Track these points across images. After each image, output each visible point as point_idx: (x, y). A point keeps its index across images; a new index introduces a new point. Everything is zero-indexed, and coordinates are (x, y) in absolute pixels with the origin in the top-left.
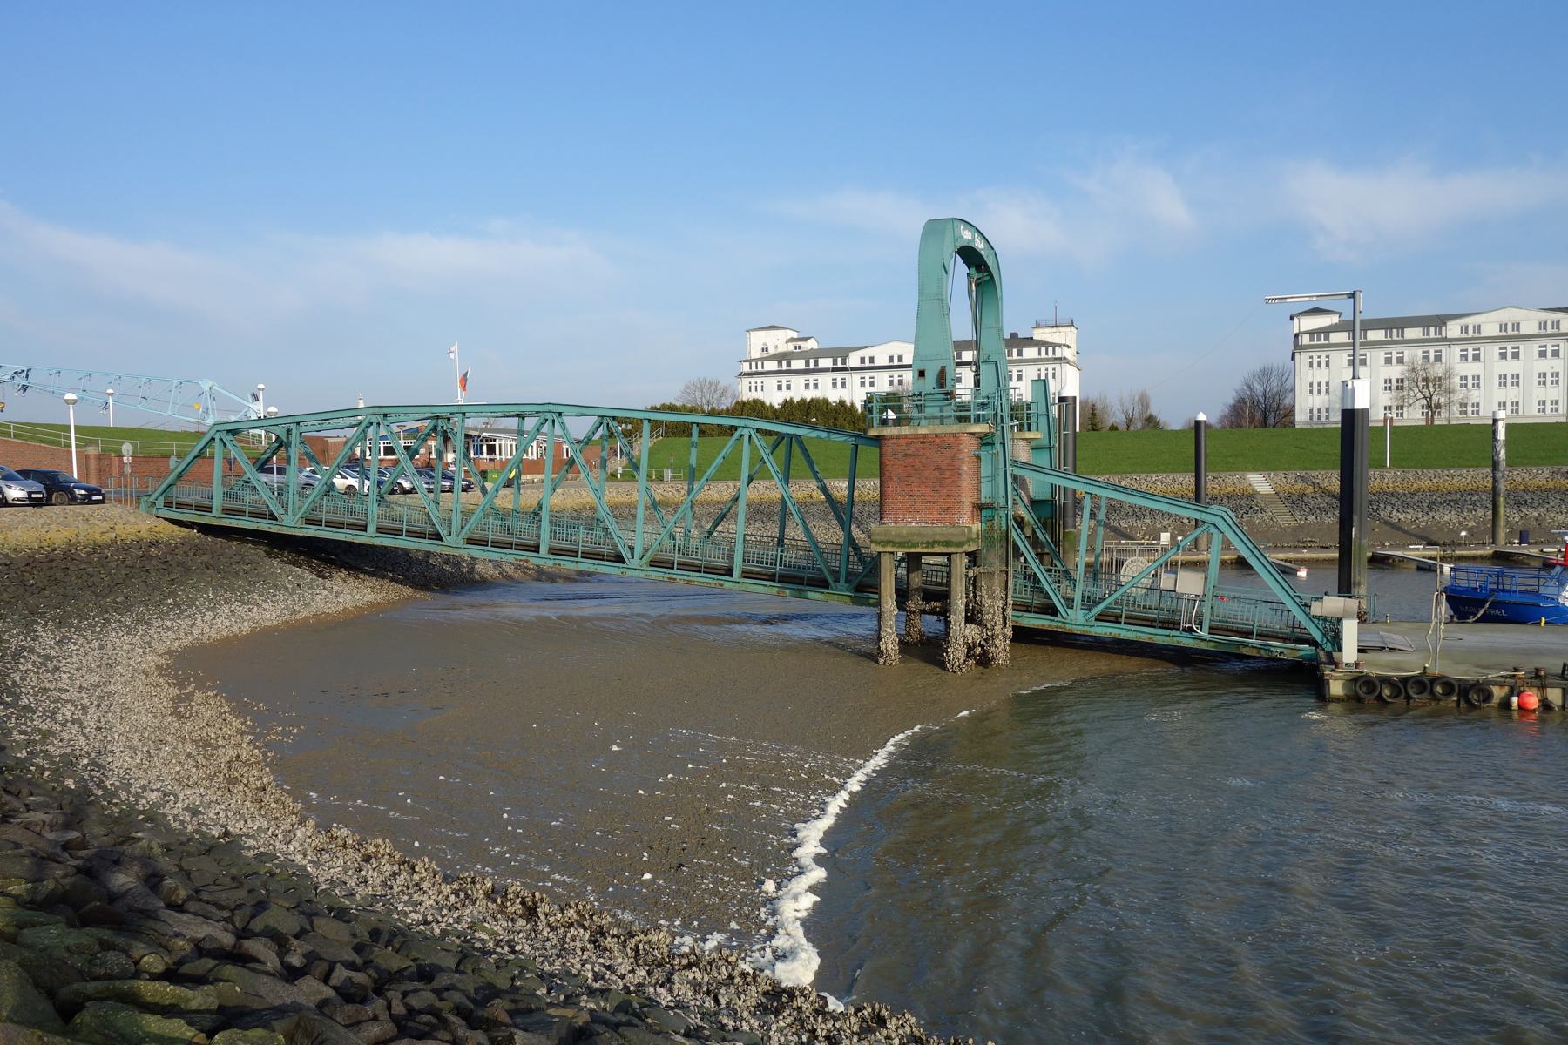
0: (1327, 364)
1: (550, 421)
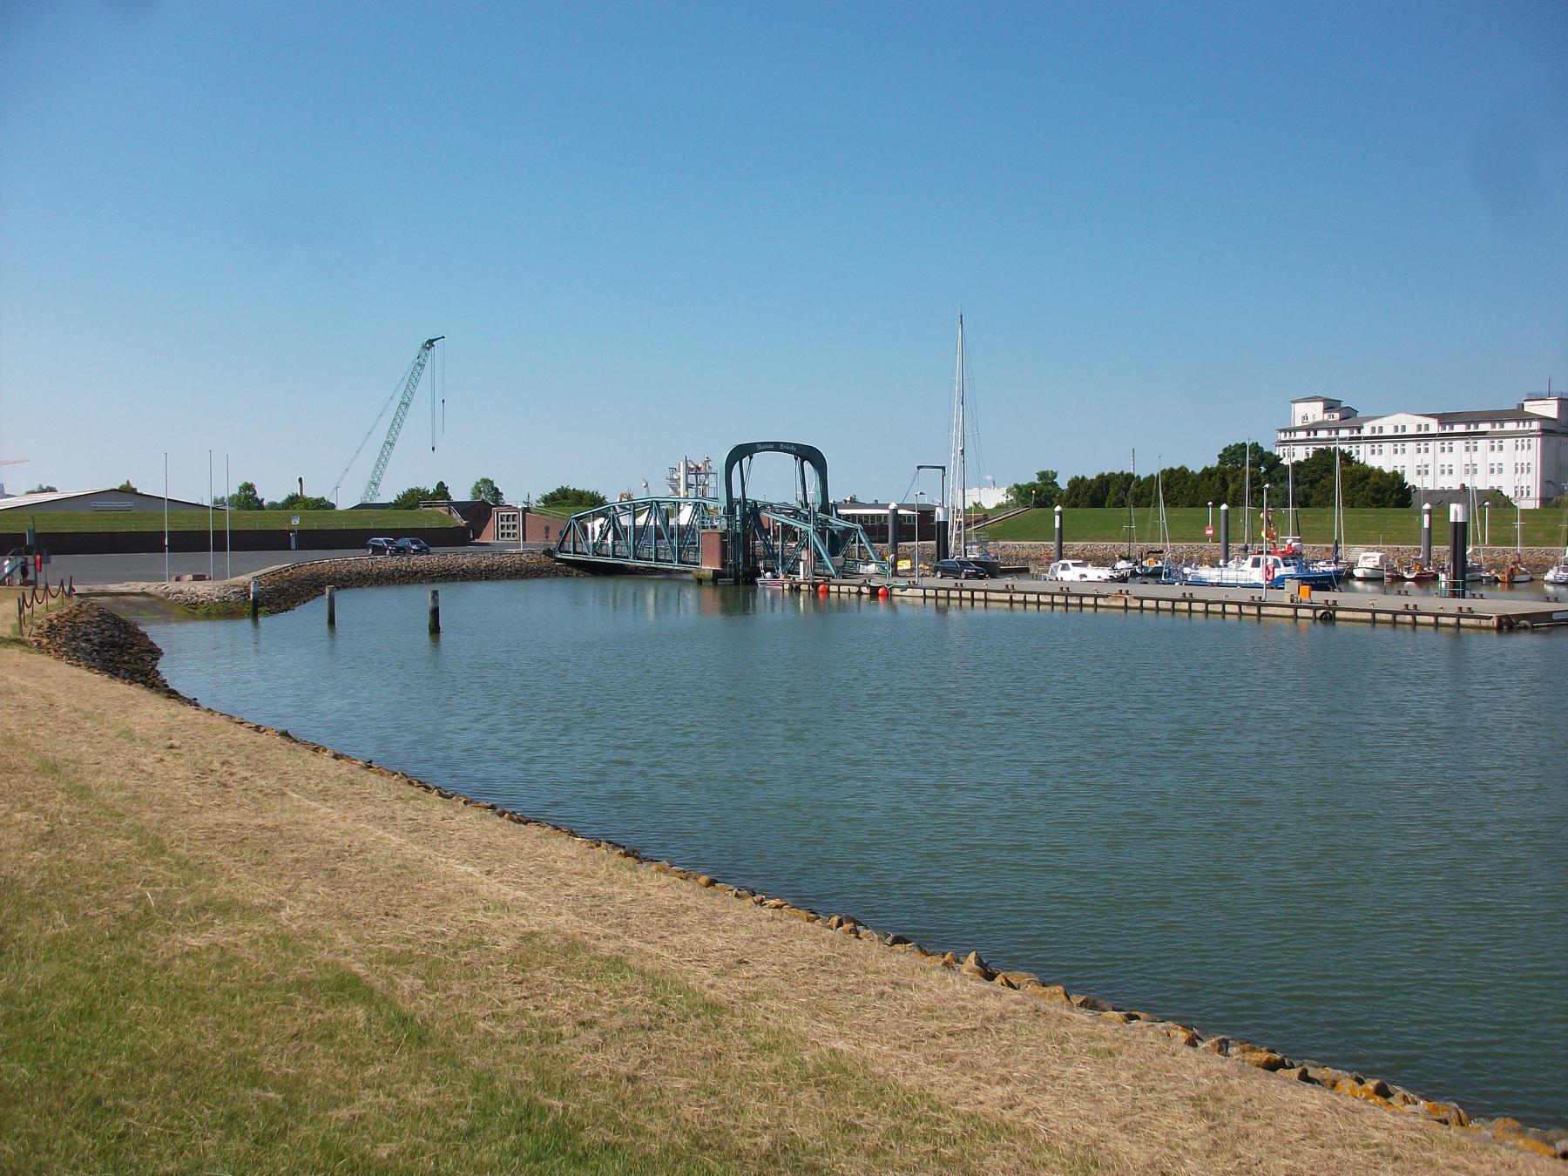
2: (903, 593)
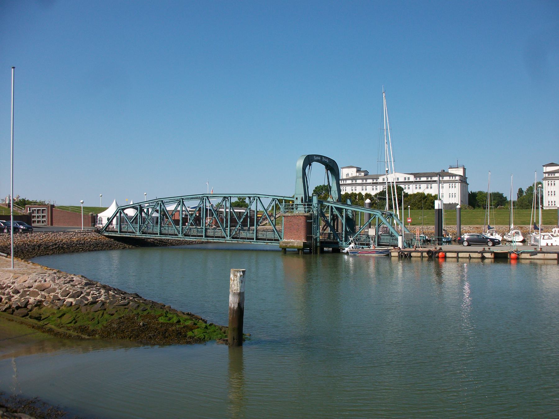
1: (256, 200)
2: (532, 257)
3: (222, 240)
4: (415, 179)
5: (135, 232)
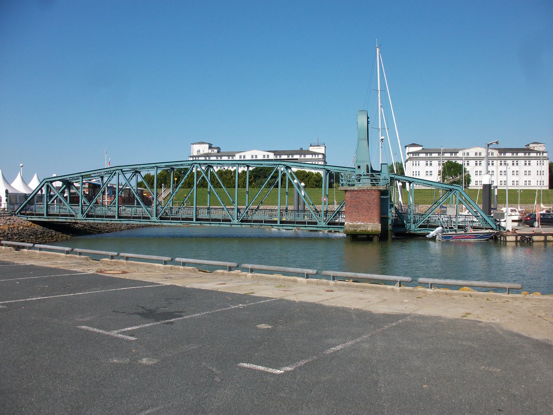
0: (419, 165)
1: (117, 174)
3: (144, 222)
4: (499, 154)
5: (75, 214)
